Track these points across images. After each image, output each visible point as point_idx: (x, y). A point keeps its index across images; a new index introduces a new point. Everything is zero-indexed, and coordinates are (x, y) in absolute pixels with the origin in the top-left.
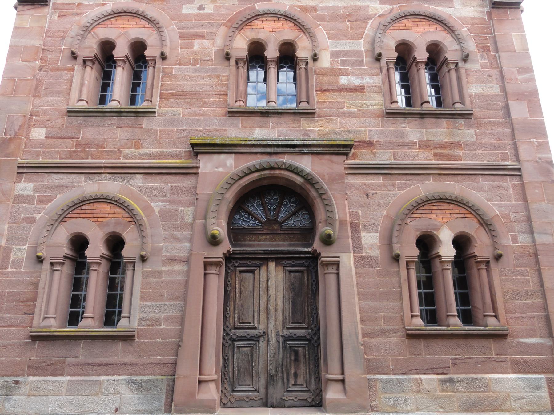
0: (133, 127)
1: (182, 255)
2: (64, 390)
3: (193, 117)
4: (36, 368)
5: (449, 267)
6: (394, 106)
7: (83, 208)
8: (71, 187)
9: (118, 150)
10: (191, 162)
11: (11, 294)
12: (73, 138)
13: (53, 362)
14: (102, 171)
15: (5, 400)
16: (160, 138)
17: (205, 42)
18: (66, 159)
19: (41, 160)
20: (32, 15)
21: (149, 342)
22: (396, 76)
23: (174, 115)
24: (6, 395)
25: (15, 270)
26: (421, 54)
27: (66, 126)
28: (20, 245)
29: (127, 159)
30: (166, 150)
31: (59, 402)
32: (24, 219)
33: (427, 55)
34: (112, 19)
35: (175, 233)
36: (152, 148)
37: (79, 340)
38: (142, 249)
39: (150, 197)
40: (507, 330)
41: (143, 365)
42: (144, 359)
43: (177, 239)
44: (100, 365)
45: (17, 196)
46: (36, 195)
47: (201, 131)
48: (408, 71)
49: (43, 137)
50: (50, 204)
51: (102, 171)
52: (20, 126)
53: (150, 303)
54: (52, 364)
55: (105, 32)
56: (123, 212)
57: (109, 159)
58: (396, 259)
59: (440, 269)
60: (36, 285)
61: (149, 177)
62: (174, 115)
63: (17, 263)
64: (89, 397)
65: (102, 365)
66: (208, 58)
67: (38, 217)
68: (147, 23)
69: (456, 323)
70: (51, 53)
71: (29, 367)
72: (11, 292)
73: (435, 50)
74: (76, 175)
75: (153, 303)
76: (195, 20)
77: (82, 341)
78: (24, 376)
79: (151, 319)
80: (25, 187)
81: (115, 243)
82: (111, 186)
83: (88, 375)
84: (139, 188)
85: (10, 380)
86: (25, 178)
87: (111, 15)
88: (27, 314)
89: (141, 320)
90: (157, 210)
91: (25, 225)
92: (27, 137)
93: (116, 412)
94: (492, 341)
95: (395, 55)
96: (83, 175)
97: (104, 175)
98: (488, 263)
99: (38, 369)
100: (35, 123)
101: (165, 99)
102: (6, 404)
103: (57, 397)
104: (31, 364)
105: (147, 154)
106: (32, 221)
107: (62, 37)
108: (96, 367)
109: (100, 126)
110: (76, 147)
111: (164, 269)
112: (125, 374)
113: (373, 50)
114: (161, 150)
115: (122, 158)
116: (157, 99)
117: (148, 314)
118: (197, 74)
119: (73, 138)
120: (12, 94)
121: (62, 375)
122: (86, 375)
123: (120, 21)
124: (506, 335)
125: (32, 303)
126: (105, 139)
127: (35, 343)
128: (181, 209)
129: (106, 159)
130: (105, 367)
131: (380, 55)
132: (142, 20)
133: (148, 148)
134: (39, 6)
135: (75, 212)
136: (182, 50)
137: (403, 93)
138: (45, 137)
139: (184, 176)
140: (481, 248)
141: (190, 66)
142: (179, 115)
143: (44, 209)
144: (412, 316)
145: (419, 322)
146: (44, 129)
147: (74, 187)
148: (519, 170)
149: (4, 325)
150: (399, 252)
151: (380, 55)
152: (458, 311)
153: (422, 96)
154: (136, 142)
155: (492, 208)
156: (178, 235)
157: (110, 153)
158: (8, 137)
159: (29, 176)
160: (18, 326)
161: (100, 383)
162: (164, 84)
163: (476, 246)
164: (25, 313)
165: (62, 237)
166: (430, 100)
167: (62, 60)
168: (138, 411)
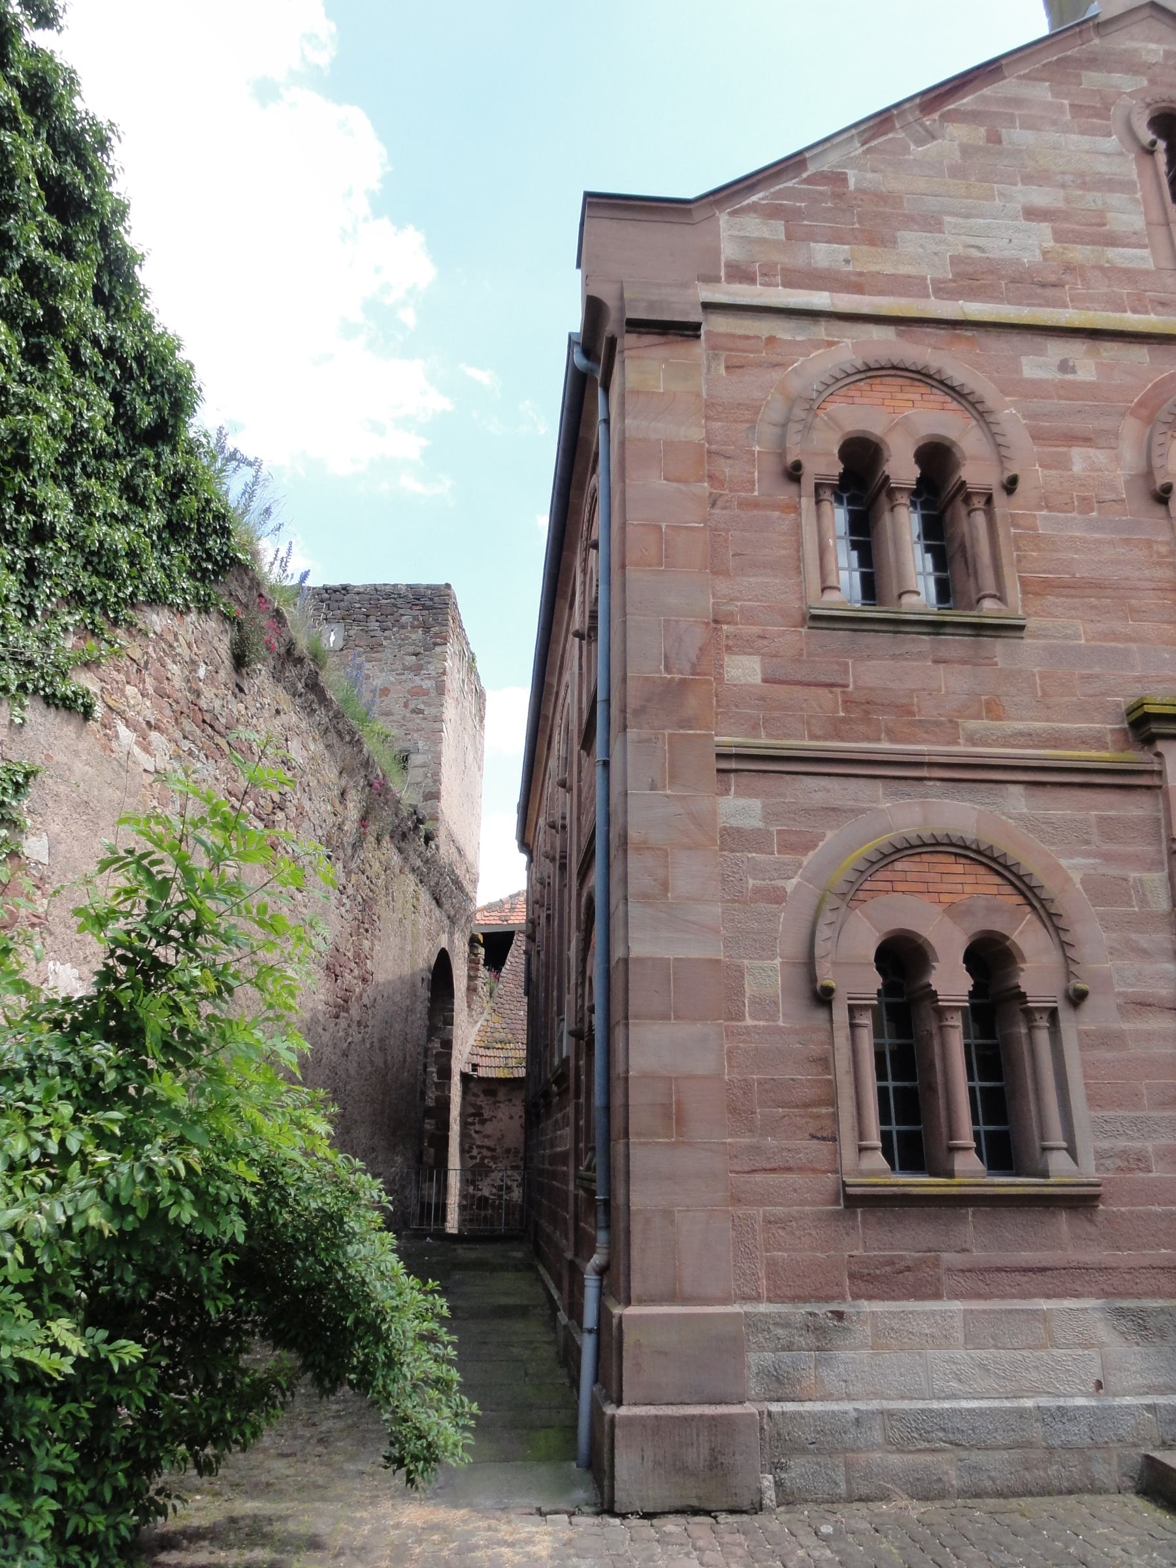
0: (975, 665)
1: (1164, 992)
2: (960, 1336)
3: (1113, 644)
4: (870, 1279)
5: (956, 1021)
6: (831, 597)
7: (898, 866)
8: (855, 812)
9: (950, 721)
10: (1135, 757)
11: (767, 1086)
12: (832, 685)
13: (910, 1263)
14: (924, 773)
15: (818, 1362)
16: (1045, 694)
17: (1099, 456)
18: (825, 739)
19: (763, 741)
20: (666, 361)
21: (1131, 1213)
22: (838, 517)
23: (1066, 637)
24: (818, 1349)
25: (762, 1023)
26: (902, 469)
27: (810, 655)
28: (761, 958)
29: (974, 745)
30: (1069, 725)
31: (954, 1367)
32: (757, 890)
33: (916, 472)
34: (862, 384)
35: (1133, 936)
36: (1032, 719)
37: (961, 1206)
38: (1069, 974)
39: (1053, 844)
40: (1099, 1185)
41: (1131, 1270)
42: (1125, 1257)
43: (1144, 953)
44: (1025, 1270)
45: (727, 832)
46: (774, 829)
47: (1138, 680)
48: (943, 512)
49: (758, 679)
50: (811, 854)
51: (924, 773)
52: (701, 649)
53: (1112, 1114)
54: (908, 1269)
55: (865, 414)
56: (997, 880)
57: (933, 743)
58: (823, 998)
59: (933, 1027)
60: (825, 1062)
61: (1038, 792)
62: (1066, 637)
63: (764, 1007)
64: (1025, 1353)
65: (1031, 1270)
66: (1113, 497)
67: (790, 885)
68: (949, 399)
69: (969, 1169)
70: (731, 462)
71: (852, 1276)
72: (766, 1081)
73: (936, 458)
74: (862, 781)
75: (1120, 1113)
76: (1060, 397)
77: (970, 1210)
78: (844, 1299)
79: (1124, 1154)
80: (741, 808)
81: (989, 957)
82: (958, 813)
83: (1003, 1297)
84: (1020, 818)
85: (821, 1309)
86: (737, 786)
87: (860, 372)
88: (818, 1138)
89: (1101, 1155)
90: (1076, 877)
91: (762, 906)
92: (720, 679)
93: (1098, 1390)
94: (1064, 1216)
95: (837, 468)
96: (879, 783)
97: (931, 783)
98: (1053, 1013)
99: (876, 1281)
100: (730, 643)
101: (1036, 594)
102: (824, 1372)
103: (945, 1354)
104: (855, 1268)
105: (1022, 734)
106: (777, 897)
107: (747, 421)
108: (1018, 1277)
109: (894, 657)
110: (846, 710)
111: (1126, 1026)
112: (1090, 1295)
113: (1149, 474)
114: (1054, 725)
115: (961, 741)
116: (1014, 592)
117: (1114, 1140)
118: (1097, 536)
119: (832, 685)
120: (660, 564)
121: (937, 1296)
122: (998, 1297)
123: (880, 388)
124: (1096, 1197)
125: (824, 1110)
126: (913, 691)
127: (855, 1213)
128: (1133, 875)
129: (924, 741)
130: (1039, 1277)
131: (797, 466)
132: (934, 390)
133: (1021, 719)
134: (679, 339)
135: (879, 876)
136: (1046, 472)
137: (855, 564)
138: (765, 681)
139: (1123, 792)
140: (1038, 976)
141: (1074, 514)
142: (1078, 637)
143: (800, 866)
144: (862, 1149)
145: (874, 1170)
146: (757, 658)
147: (863, 811)
148: (1160, 773)
149: (768, 1166)
150: (833, 984)
151: (797, 466)
152: (976, 1135)
153: (901, 577)
154: (988, 703)
155: (1067, 870)
156: (1143, 940)
157: (931, 727)
158: (677, 676)
159: (745, 779)
160: (801, 1169)
161: (1044, 1317)
162: (1025, 557)
163: (1022, 970)
164: (813, 1137)
165: (862, 938)
166: (921, 589)
167: (761, 481)
168: (1149, 1387)
